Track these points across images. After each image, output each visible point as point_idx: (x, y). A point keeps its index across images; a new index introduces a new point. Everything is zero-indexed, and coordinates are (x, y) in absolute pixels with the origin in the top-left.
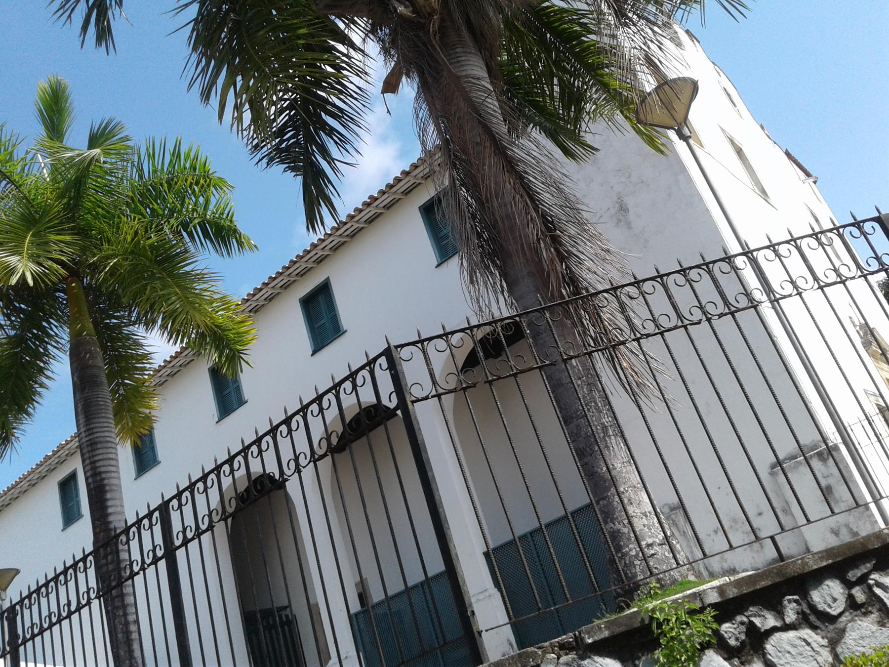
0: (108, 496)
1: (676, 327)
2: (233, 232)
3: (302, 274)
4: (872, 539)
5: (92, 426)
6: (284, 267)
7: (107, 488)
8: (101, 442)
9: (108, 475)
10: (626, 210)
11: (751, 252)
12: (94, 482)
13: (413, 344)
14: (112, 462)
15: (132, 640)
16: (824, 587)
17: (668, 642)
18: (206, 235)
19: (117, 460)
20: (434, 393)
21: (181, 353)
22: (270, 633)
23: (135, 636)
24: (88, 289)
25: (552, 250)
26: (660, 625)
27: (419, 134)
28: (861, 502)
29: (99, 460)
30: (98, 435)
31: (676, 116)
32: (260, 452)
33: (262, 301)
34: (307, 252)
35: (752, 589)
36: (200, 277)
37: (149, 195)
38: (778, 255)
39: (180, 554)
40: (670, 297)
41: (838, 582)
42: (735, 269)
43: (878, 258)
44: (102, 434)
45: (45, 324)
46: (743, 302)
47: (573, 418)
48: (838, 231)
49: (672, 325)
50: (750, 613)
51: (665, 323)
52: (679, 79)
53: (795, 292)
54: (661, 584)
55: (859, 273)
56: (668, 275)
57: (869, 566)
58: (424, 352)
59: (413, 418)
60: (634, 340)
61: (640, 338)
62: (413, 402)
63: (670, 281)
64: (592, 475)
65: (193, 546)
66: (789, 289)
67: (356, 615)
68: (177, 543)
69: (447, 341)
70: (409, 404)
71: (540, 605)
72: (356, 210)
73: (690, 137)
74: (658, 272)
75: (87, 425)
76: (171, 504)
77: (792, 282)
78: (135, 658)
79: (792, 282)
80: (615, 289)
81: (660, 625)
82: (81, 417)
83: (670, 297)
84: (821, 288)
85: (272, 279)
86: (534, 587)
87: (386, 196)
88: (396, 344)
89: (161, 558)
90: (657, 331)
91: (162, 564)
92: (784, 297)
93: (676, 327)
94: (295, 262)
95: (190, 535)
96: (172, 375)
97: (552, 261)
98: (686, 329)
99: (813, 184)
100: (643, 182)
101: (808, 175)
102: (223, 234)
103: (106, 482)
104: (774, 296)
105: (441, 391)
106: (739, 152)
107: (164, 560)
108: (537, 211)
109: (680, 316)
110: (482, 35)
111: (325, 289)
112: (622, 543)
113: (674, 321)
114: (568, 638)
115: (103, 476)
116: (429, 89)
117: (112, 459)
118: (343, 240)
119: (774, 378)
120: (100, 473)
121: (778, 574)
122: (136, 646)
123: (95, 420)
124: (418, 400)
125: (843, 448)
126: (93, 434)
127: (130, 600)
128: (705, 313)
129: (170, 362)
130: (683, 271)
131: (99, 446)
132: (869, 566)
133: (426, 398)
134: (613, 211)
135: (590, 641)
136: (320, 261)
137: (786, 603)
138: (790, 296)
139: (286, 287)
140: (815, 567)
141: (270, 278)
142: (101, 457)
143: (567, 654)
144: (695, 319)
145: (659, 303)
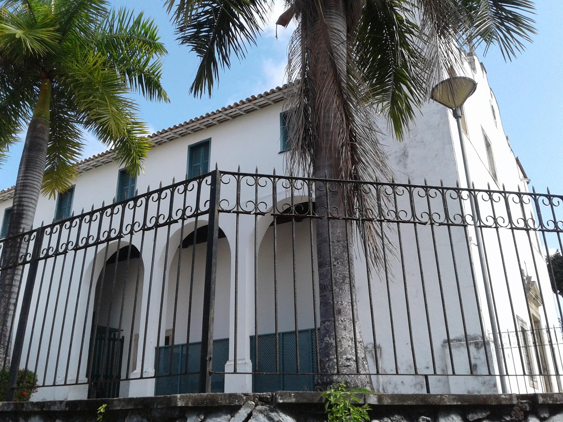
0: (24, 221)
1: (409, 222)
2: (158, 86)
3: (196, 131)
4: (492, 398)
5: (28, 175)
6: (185, 122)
7: (24, 216)
8: (30, 187)
9: (28, 208)
10: (407, 156)
11: (475, 190)
12: (17, 210)
13: (233, 174)
14: (33, 201)
15: (8, 314)
16: (450, 418)
17: (333, 420)
18: (140, 81)
19: (36, 201)
20: (235, 210)
21: (105, 154)
22: (101, 343)
23: (11, 313)
24: (54, 91)
25: (349, 153)
26: (331, 406)
27: (289, 55)
28: (492, 373)
29: (25, 197)
30: (30, 181)
31: (456, 101)
32: (112, 214)
33: (164, 139)
34: (203, 118)
35: (400, 404)
36: (127, 104)
37: (110, 44)
38: (491, 199)
39: (41, 263)
40: (412, 201)
41: (460, 418)
42: (460, 198)
43: (555, 222)
44: (32, 182)
45: (21, 103)
46: (459, 221)
47: (326, 264)
48: (535, 197)
49: (407, 219)
50: (394, 419)
51: (402, 216)
52: (464, 78)
53: (494, 226)
54: (347, 386)
55: (540, 228)
56: (415, 187)
57: (484, 415)
58: (238, 182)
59: (215, 221)
60: (378, 221)
61: (383, 221)
62: (219, 211)
63: (415, 191)
64: (326, 304)
65: (50, 261)
66: (491, 222)
67: (160, 348)
68: (42, 256)
69: (256, 180)
70: (216, 211)
71: (257, 369)
72: (241, 101)
73: (461, 117)
74: (409, 183)
75: (25, 173)
76: (46, 230)
77: (495, 219)
78: (6, 326)
79: (495, 219)
80: (378, 184)
81: (331, 406)
82: (23, 167)
83: (412, 201)
84: (512, 229)
85: (176, 127)
86: (257, 355)
87: (262, 99)
88: (222, 170)
89: (28, 262)
90: (396, 220)
91: (27, 266)
92: (486, 226)
93: (409, 222)
94: (193, 122)
95: (51, 253)
96: (96, 166)
97: (346, 161)
98: (415, 225)
99: (526, 183)
100: (423, 142)
101: (525, 176)
102: (152, 85)
103: (25, 212)
104: (480, 223)
105: (240, 210)
106: (488, 146)
107: (29, 264)
108: (347, 125)
109: (414, 215)
110: (351, 7)
111: (206, 144)
112: (331, 352)
113: (409, 217)
114: (267, 395)
115: (25, 208)
116: (306, 29)
117: (34, 199)
118: (228, 118)
119: (462, 282)
120: (23, 205)
121: (422, 400)
122: (10, 319)
123: (31, 172)
124: (223, 211)
125: (492, 346)
126: (27, 179)
127: (15, 290)
128: (431, 218)
129: (97, 158)
130: (426, 188)
131: (28, 188)
132: (484, 415)
133: (229, 212)
134: (398, 154)
135: (281, 401)
136: (209, 126)
137: (421, 420)
138: (490, 227)
139: (183, 135)
140: (448, 404)
141: (175, 126)
142: (27, 196)
143: (262, 405)
144: (423, 220)
145: (403, 201)
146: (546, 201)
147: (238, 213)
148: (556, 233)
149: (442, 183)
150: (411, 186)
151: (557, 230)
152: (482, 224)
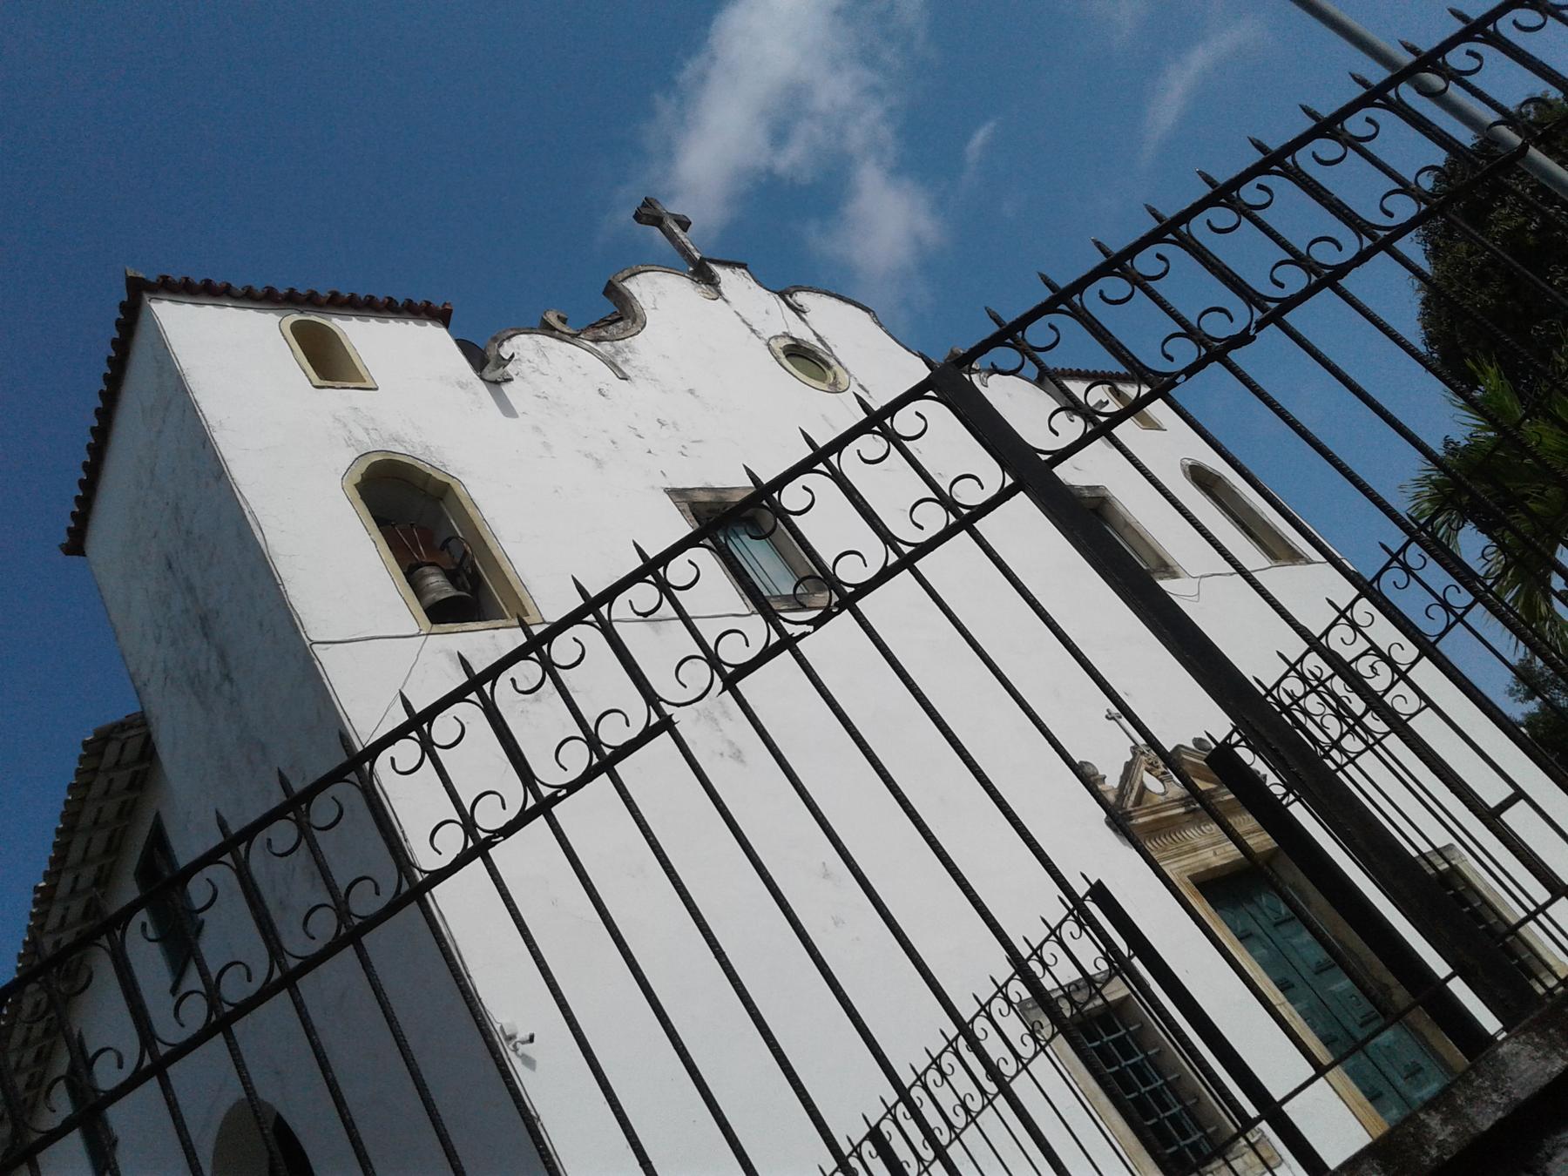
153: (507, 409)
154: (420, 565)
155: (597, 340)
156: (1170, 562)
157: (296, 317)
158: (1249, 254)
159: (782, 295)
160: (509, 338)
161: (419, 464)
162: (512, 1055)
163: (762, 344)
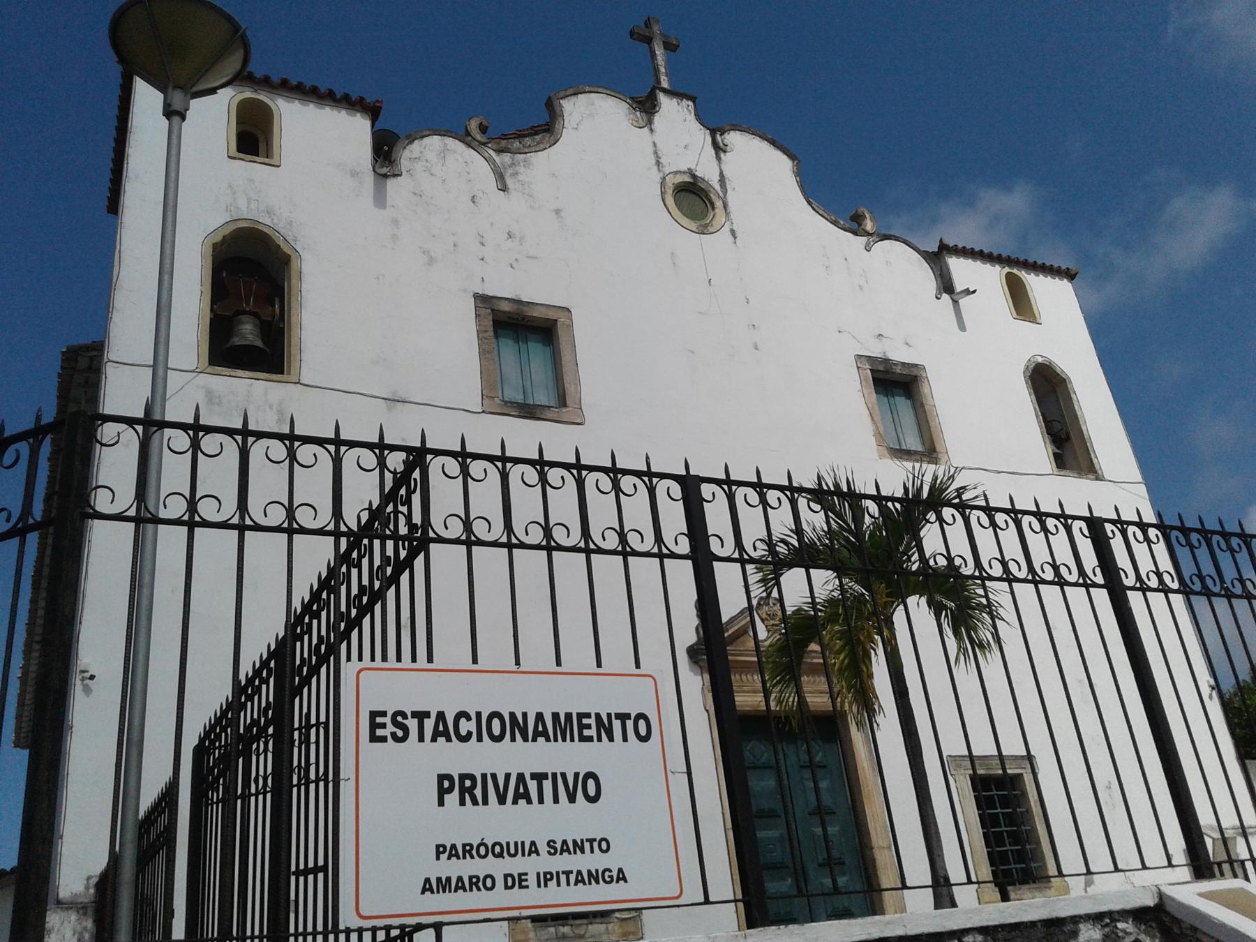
4: (824, 915)
63: (350, 457)
93: (648, 554)
105: (248, 522)
109: (659, 539)
146: (753, 497)
147: (242, 529)
148: (739, 565)
149: (758, 472)
150: (504, 459)
151: (1248, 597)
152: (514, 541)
153: (380, 199)
154: (244, 313)
155: (500, 151)
156: (938, 448)
157: (248, 94)
158: (602, 511)
159: (713, 133)
160: (422, 137)
161: (275, 236)
162: (78, 682)
163: (657, 177)
